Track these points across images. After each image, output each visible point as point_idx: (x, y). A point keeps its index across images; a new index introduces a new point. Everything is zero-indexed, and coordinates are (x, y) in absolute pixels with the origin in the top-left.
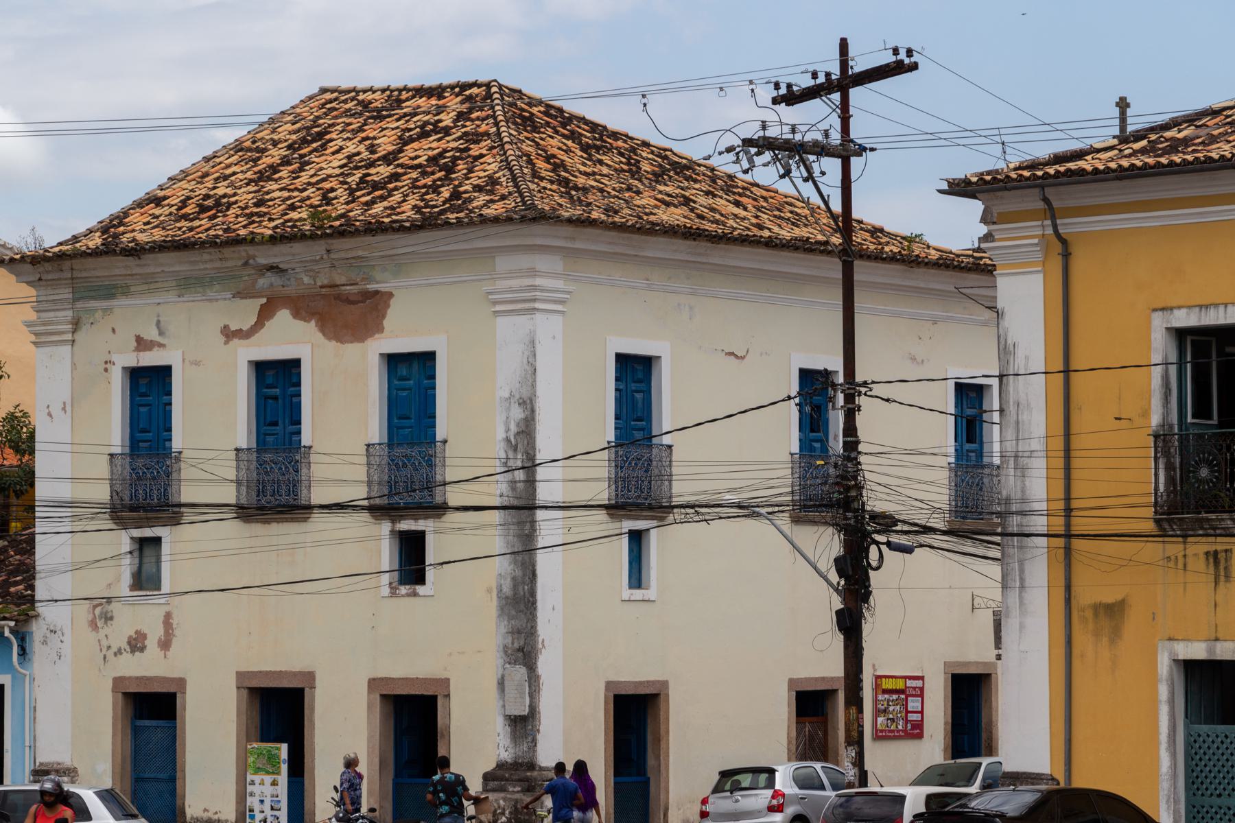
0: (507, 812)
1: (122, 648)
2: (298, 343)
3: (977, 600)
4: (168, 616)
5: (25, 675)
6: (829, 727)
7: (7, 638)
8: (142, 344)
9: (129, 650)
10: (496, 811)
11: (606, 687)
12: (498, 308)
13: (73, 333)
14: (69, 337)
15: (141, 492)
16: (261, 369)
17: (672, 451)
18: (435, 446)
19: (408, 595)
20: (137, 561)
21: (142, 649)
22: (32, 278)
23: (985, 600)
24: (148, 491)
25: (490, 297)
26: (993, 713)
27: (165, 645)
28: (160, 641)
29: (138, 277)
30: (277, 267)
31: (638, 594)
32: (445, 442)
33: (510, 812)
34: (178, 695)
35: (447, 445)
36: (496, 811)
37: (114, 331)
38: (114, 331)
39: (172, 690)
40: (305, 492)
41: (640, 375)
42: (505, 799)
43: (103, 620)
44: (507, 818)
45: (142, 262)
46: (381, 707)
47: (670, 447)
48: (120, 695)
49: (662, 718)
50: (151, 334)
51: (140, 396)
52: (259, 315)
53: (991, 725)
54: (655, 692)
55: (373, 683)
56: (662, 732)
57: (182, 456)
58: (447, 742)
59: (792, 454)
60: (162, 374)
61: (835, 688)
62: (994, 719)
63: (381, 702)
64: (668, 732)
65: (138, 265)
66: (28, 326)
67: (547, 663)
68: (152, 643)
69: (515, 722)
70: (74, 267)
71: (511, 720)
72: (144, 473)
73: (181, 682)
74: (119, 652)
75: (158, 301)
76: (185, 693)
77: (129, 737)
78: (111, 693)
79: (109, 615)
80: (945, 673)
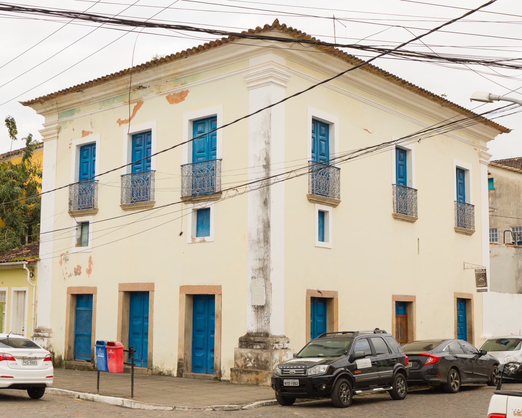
0: (252, 360)
1: (72, 273)
2: (221, 314)
3: (466, 265)
4: (90, 258)
5: (33, 286)
6: (408, 320)
7: (25, 269)
8: (85, 134)
9: (74, 274)
10: (246, 359)
11: (307, 292)
12: (250, 85)
13: (58, 133)
14: (56, 135)
15: (81, 200)
16: (135, 137)
17: (340, 171)
18: (216, 162)
19: (201, 242)
20: (80, 233)
21: (79, 274)
22: (42, 111)
23: (471, 265)
24: (84, 199)
25: (246, 80)
26: (472, 317)
27: (89, 271)
28: (87, 269)
29: (83, 103)
30: (142, 86)
31: (322, 244)
32: (221, 160)
33: (254, 360)
34: (93, 295)
35: (222, 161)
36: (246, 359)
37: (73, 130)
38: (73, 130)
39: (91, 293)
40: (152, 193)
41: (323, 132)
42: (251, 352)
43: (65, 260)
44: (252, 363)
45: (84, 94)
46: (186, 301)
47: (339, 169)
48: (70, 295)
49: (334, 311)
50: (88, 129)
51: (84, 158)
52: (133, 112)
53: (471, 322)
54: (331, 297)
55: (182, 288)
56: (335, 319)
57: (99, 182)
58: (220, 320)
59: (393, 185)
60: (93, 145)
61: (412, 301)
62: (472, 320)
63: (186, 298)
64: (337, 319)
65: (83, 96)
66: (41, 132)
67: (274, 276)
68: (83, 271)
69: (258, 309)
70: (58, 103)
71: (255, 308)
72: (83, 191)
73: (95, 289)
74: (70, 275)
75: (91, 113)
76: (96, 294)
77: (74, 315)
78: (66, 294)
79: (67, 259)
80: (454, 297)
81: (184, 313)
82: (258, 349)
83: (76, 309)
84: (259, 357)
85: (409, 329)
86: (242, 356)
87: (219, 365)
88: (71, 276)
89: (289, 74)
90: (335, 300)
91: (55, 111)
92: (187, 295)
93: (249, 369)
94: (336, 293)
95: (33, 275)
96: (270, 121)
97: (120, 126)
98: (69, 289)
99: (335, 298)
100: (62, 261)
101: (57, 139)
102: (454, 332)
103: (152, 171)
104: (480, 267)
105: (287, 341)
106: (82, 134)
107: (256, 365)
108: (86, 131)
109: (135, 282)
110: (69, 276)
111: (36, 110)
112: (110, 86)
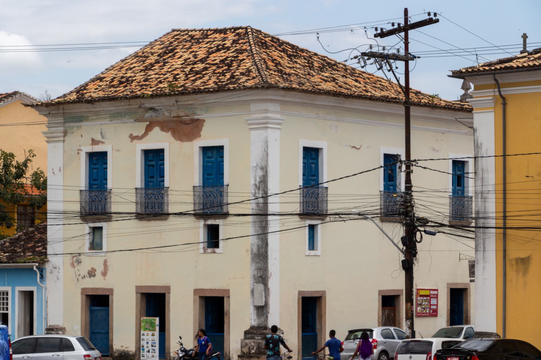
0: (255, 348)
1: (85, 275)
3: (462, 256)
8: (94, 142)
9: (88, 276)
12: (251, 127)
13: (64, 137)
16: (147, 153)
17: (327, 190)
18: (224, 187)
19: (211, 253)
20: (92, 237)
21: (94, 276)
22: (45, 113)
25: (248, 122)
27: (104, 274)
28: (102, 272)
29: (92, 112)
30: (154, 108)
31: (312, 253)
32: (228, 185)
33: (256, 348)
36: (250, 347)
37: (82, 136)
38: (82, 136)
39: (107, 294)
41: (314, 157)
42: (254, 342)
43: (77, 263)
47: (327, 188)
50: (98, 138)
54: (320, 296)
55: (196, 291)
56: (323, 313)
59: (380, 191)
60: (103, 155)
61: (399, 294)
64: (325, 313)
65: (93, 107)
67: (273, 283)
68: (98, 273)
71: (257, 308)
73: (111, 290)
74: (84, 277)
79: (79, 261)
80: (447, 288)
81: (198, 312)
82: (260, 339)
83: (90, 308)
84: (260, 345)
85: (397, 320)
86: (247, 345)
87: (228, 353)
88: (85, 278)
89: (284, 118)
90: (323, 298)
91: (60, 114)
92: (200, 297)
93: (253, 355)
94: (324, 292)
95: (42, 277)
96: (267, 148)
97: (131, 142)
98: (83, 290)
99: (323, 296)
100: (74, 263)
101: (63, 142)
102: (446, 320)
103: (166, 187)
104: (473, 258)
105: (281, 333)
106: (91, 142)
107: (257, 352)
108: (96, 139)
109: (152, 285)
110: (82, 278)
111: (39, 111)
112: (123, 104)
